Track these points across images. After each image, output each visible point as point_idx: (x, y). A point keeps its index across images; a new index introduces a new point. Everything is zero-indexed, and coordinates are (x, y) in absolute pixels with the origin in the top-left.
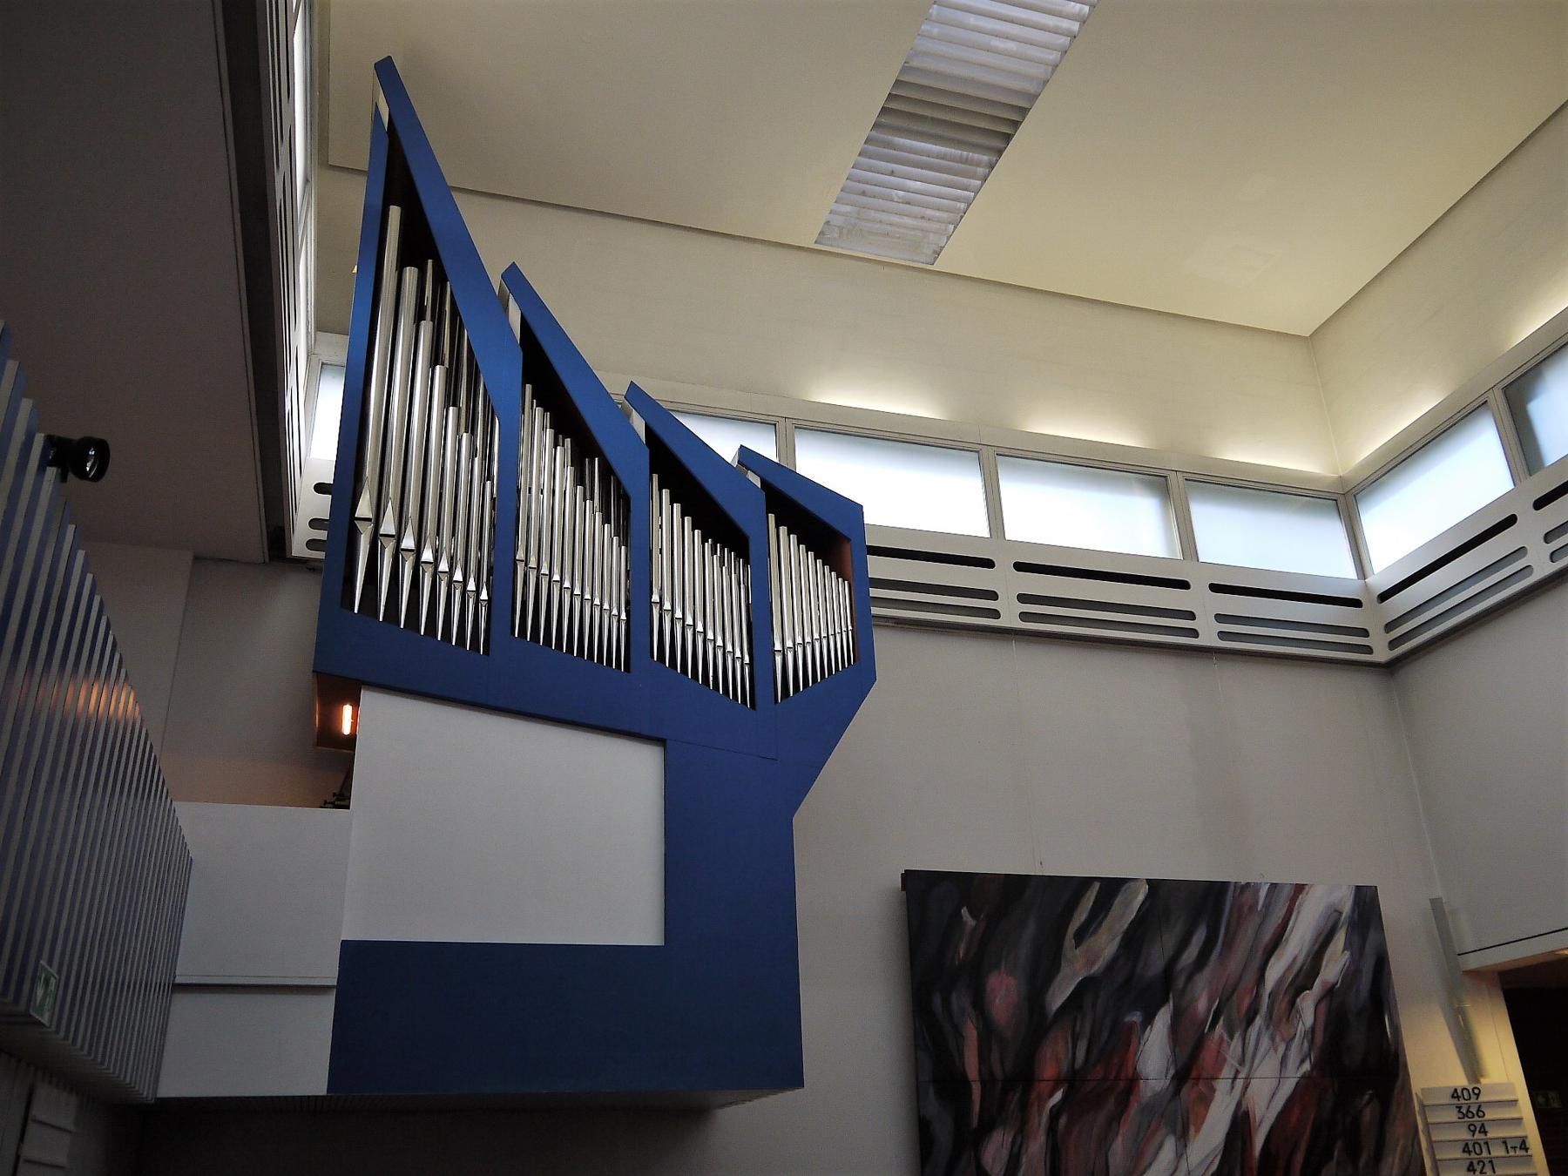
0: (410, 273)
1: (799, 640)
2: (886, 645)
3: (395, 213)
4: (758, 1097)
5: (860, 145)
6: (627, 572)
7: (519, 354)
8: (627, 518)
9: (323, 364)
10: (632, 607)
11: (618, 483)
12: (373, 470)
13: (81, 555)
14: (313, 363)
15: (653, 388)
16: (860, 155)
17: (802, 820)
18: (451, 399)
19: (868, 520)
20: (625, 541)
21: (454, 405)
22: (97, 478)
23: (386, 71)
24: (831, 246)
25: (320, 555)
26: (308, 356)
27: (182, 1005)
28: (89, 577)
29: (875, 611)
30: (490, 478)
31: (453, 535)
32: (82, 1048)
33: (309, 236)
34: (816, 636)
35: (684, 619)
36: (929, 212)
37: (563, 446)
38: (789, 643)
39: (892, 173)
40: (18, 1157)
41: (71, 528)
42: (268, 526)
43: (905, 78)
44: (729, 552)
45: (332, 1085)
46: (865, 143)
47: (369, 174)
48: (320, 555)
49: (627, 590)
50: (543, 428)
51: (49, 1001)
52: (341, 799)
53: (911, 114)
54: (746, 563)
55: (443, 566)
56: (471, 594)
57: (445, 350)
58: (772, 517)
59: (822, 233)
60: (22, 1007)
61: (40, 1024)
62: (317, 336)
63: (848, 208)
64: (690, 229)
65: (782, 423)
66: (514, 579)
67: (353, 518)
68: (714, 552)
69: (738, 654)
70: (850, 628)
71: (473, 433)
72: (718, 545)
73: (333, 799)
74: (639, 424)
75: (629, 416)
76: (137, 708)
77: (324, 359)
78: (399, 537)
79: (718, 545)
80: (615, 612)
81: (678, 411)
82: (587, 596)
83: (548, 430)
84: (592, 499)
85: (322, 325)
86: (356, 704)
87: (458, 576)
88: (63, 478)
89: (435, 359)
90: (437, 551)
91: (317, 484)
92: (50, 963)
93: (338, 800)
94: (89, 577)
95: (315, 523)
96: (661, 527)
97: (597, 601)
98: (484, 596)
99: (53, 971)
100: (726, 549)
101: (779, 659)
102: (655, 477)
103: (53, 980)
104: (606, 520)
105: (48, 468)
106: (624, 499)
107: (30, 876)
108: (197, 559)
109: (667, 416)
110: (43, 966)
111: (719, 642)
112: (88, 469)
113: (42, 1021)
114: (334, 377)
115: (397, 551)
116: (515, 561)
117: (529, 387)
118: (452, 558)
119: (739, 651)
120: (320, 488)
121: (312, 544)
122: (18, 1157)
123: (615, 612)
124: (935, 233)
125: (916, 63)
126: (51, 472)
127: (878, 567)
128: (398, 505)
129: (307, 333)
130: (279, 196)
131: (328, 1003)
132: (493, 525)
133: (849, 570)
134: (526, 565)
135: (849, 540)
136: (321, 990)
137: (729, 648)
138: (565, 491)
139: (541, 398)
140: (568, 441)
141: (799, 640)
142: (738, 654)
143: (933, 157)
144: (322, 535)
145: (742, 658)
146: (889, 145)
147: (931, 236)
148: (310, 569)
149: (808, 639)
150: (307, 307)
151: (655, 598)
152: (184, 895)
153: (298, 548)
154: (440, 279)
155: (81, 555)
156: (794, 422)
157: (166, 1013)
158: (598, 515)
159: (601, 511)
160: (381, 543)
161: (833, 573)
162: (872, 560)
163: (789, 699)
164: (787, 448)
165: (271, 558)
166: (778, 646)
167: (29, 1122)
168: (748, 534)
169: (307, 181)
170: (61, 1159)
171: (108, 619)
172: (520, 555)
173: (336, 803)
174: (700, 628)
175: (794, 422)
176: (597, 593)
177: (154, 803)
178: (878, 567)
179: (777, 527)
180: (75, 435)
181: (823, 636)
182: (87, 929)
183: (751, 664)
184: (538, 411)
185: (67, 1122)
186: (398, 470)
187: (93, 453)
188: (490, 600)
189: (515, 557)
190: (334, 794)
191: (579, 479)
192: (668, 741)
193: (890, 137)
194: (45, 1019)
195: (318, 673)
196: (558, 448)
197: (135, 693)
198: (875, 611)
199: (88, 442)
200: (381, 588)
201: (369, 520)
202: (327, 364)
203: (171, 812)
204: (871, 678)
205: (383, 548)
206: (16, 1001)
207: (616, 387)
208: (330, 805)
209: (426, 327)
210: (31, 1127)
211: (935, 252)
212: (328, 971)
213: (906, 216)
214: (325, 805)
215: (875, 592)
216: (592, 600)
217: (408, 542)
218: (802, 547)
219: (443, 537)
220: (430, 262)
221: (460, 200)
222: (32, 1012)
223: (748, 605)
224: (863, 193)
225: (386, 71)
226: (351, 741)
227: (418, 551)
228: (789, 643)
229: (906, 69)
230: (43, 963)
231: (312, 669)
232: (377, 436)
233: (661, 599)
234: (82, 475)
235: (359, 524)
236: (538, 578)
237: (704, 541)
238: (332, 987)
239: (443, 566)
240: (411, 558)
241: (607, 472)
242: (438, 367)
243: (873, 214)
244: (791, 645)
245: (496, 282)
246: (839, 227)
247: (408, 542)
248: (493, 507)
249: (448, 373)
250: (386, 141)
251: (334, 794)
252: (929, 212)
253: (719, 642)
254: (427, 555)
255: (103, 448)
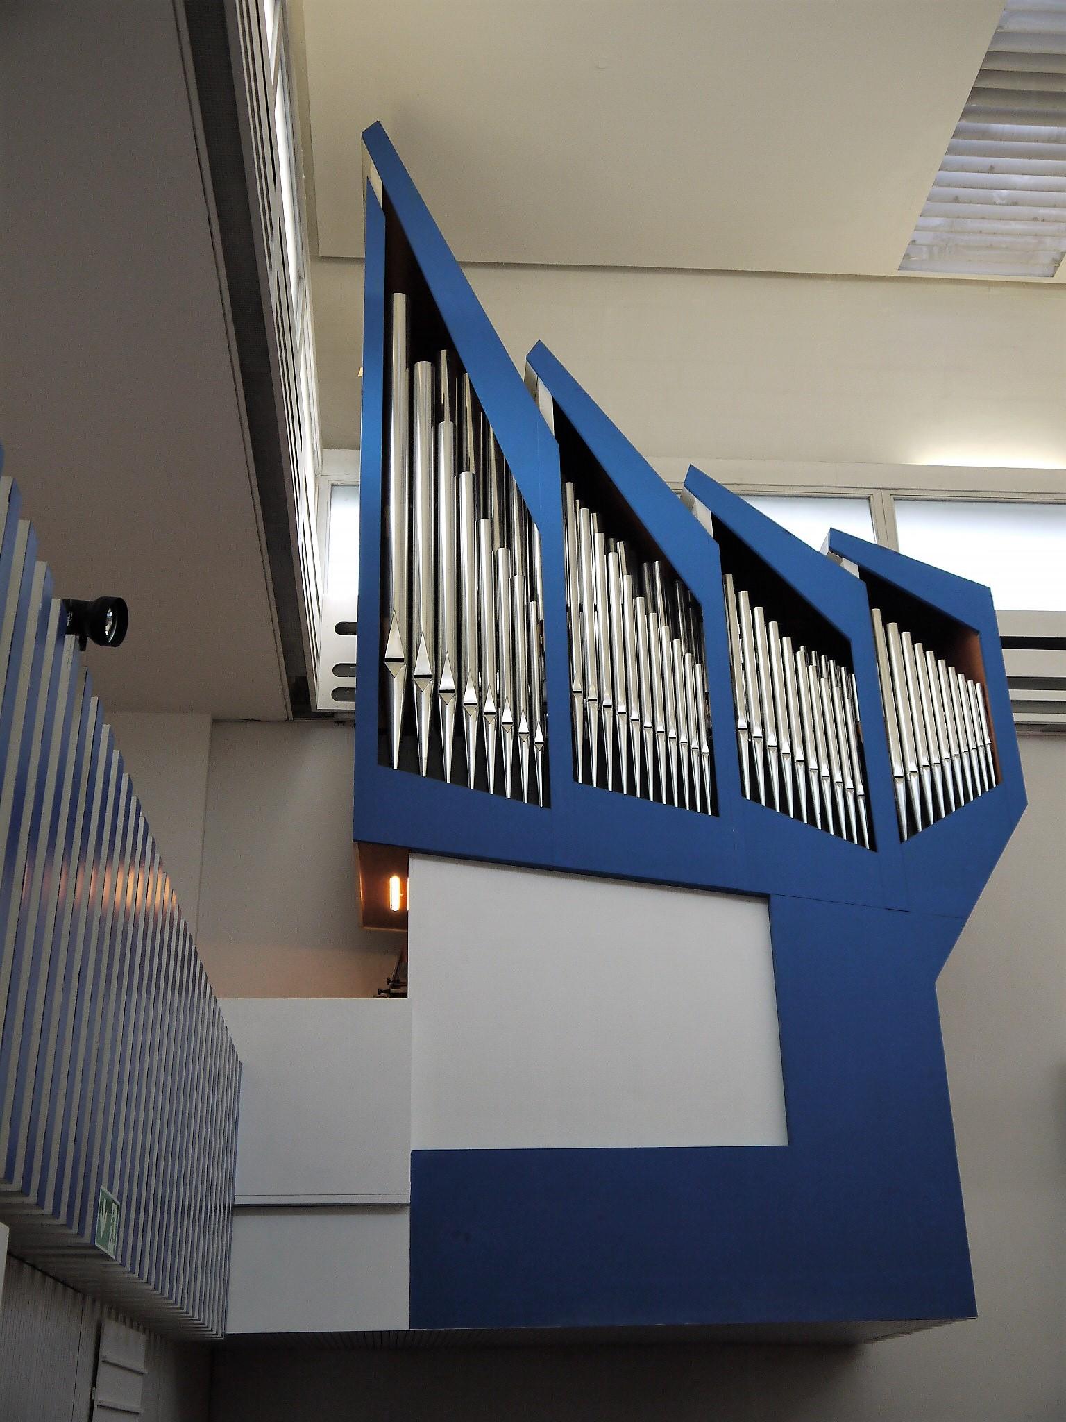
0: (423, 368)
1: (924, 761)
2: (1032, 756)
3: (399, 300)
4: (919, 1329)
5: (947, 140)
6: (706, 695)
7: (555, 448)
8: (698, 630)
9: (333, 486)
10: (715, 738)
11: (685, 588)
12: (400, 602)
13: (105, 730)
14: (322, 487)
15: (718, 471)
16: (948, 152)
17: (945, 984)
18: (481, 510)
19: (997, 606)
20: (699, 659)
21: (485, 517)
22: (117, 641)
23: (375, 138)
24: (921, 270)
25: (350, 706)
26: (316, 480)
27: (245, 1226)
28: (116, 754)
29: (1018, 717)
30: (533, 597)
31: (498, 669)
32: (148, 1282)
33: (306, 342)
34: (945, 754)
35: (778, 746)
36: (1043, 211)
37: (616, 551)
38: (912, 766)
39: (991, 169)
40: (92, 1402)
41: (94, 700)
42: (288, 677)
43: (998, 48)
44: (828, 660)
45: (413, 1322)
46: (954, 136)
47: (367, 261)
48: (350, 706)
49: (707, 717)
50: (591, 533)
51: (113, 1231)
52: (396, 987)
53: (1007, 91)
54: (850, 671)
55: (490, 707)
56: (524, 737)
57: (469, 455)
58: (877, 613)
59: (907, 256)
60: (87, 1239)
61: (106, 1257)
62: (324, 454)
63: (937, 221)
64: (776, 274)
65: (876, 496)
66: (572, 713)
67: (382, 659)
68: (808, 661)
69: (849, 784)
70: (987, 741)
71: (510, 546)
72: (813, 652)
73: (388, 987)
74: (704, 516)
75: (690, 507)
76: (174, 897)
77: (334, 480)
78: (436, 677)
79: (823, 657)
80: (694, 744)
81: (751, 495)
82: (660, 728)
83: (597, 534)
84: (655, 610)
85: (328, 442)
86: (404, 874)
87: (507, 717)
88: (82, 645)
89: (459, 466)
90: (480, 689)
91: (337, 625)
92: (110, 1189)
93: (393, 987)
94: (116, 754)
95: (340, 670)
96: (741, 637)
97: (672, 733)
98: (539, 737)
99: (114, 1197)
100: (823, 657)
101: (900, 787)
102: (729, 577)
103: (114, 1207)
104: (674, 635)
105: (67, 636)
106: (694, 606)
107: (82, 1096)
108: (215, 721)
109: (736, 502)
110: (103, 1192)
111: (825, 772)
112: (107, 633)
113: (109, 1254)
114: (346, 500)
115: (436, 694)
116: (572, 692)
117: (570, 486)
118: (498, 696)
119: (849, 778)
120: (342, 629)
121: (338, 694)
122: (92, 1402)
123: (694, 744)
124: (1053, 236)
125: (1012, 26)
126: (71, 640)
127: (1017, 663)
128: (432, 640)
129: (313, 452)
130: (274, 299)
131: (402, 1223)
132: (542, 653)
133: (980, 670)
134: (585, 697)
135: (977, 632)
136: (391, 1208)
137: (838, 778)
138: (623, 605)
139: (587, 498)
140: (621, 545)
141: (924, 761)
142: (849, 784)
143: (1043, 142)
144: (350, 682)
145: (855, 789)
146: (985, 135)
147: (1048, 240)
148: (338, 723)
149: (935, 759)
150: (311, 423)
151: (742, 723)
152: (236, 1102)
153: (324, 699)
154: (457, 370)
155: (105, 730)
156: (893, 492)
157: (229, 1236)
158: (665, 630)
159: (667, 624)
160: (416, 684)
161: (771, 624)
162: (1007, 653)
163: (917, 835)
164: (885, 523)
165: (296, 714)
166: (898, 771)
167: (101, 1365)
168: (850, 637)
169: (300, 278)
170: (136, 1406)
171: (138, 800)
172: (577, 686)
173: (393, 991)
174: (799, 755)
175: (893, 492)
176: (671, 723)
177: (199, 1002)
178: (1017, 663)
179: (885, 624)
180: (90, 596)
181: (953, 754)
182: (143, 1155)
183: (867, 796)
184: (584, 512)
185: (139, 1365)
186: (428, 596)
187: (111, 614)
188: (546, 739)
189: (571, 689)
190: (389, 981)
191: (638, 589)
192: (773, 898)
193: (986, 125)
194: (110, 1252)
195: (360, 843)
196: (611, 554)
197: (170, 879)
198: (1018, 717)
199: (105, 603)
200: (421, 740)
201: (401, 660)
202: (337, 485)
203: (215, 1012)
204: (1021, 803)
205: (419, 691)
206: (81, 1233)
207: (672, 473)
208: (386, 994)
209: (446, 428)
210: (102, 1368)
211: (1054, 260)
212: (400, 1188)
213: (1015, 220)
214: (380, 994)
215: (1015, 694)
216: (666, 732)
217: (448, 682)
218: (918, 646)
219: (485, 671)
220: (443, 353)
221: (471, 276)
222: (97, 1244)
223: (856, 724)
224: (956, 200)
225: (375, 138)
226: (402, 919)
227: (459, 691)
228: (912, 766)
229: (1000, 36)
230: (104, 1188)
231: (352, 839)
232: (402, 561)
233: (764, 733)
234: (101, 639)
235: (391, 667)
236: (600, 712)
237: (795, 649)
238: (407, 1204)
239: (490, 707)
240: (452, 700)
241: (670, 576)
242: (463, 475)
243: (971, 224)
244: (915, 769)
245: (521, 365)
246: (928, 246)
247: (448, 682)
248: (541, 633)
249: (476, 478)
250: (382, 219)
251: (389, 981)
252: (1043, 211)
253: (825, 772)
254: (470, 695)
255: (120, 607)
